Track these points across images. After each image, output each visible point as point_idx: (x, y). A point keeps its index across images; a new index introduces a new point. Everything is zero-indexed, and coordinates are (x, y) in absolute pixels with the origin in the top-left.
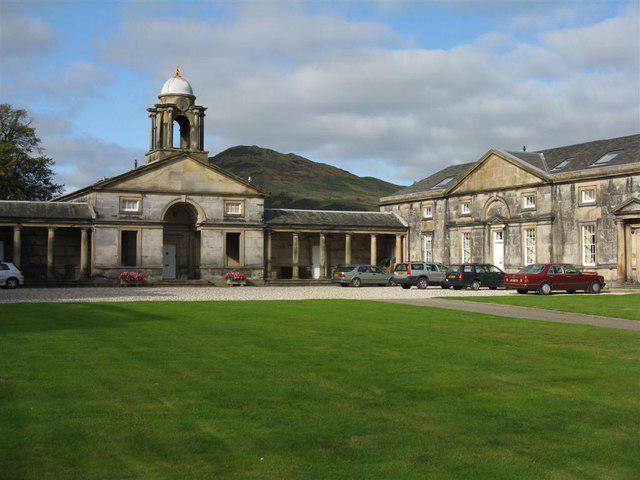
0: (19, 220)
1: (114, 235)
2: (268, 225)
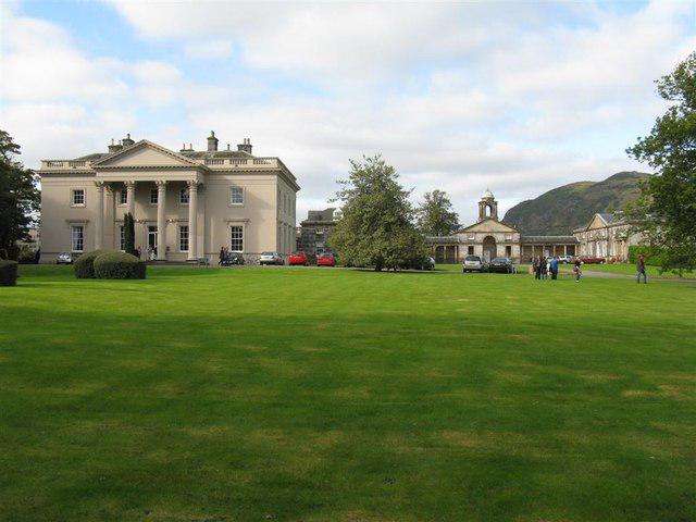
0: (565, 242)
1: (466, 248)
2: (523, 245)
